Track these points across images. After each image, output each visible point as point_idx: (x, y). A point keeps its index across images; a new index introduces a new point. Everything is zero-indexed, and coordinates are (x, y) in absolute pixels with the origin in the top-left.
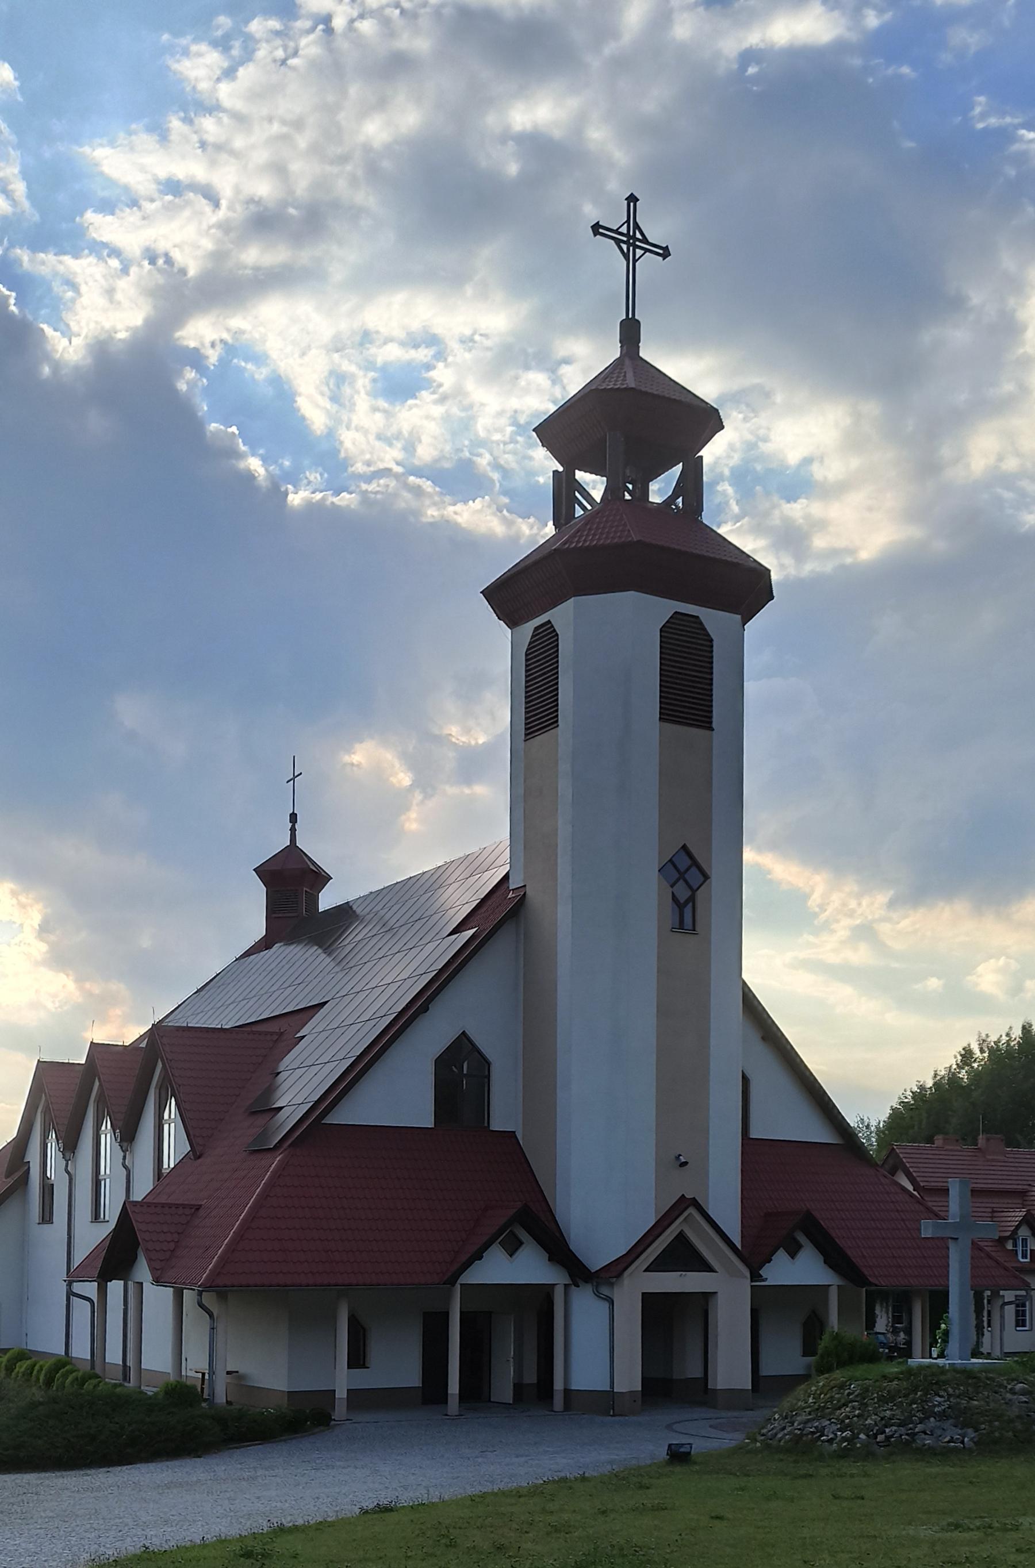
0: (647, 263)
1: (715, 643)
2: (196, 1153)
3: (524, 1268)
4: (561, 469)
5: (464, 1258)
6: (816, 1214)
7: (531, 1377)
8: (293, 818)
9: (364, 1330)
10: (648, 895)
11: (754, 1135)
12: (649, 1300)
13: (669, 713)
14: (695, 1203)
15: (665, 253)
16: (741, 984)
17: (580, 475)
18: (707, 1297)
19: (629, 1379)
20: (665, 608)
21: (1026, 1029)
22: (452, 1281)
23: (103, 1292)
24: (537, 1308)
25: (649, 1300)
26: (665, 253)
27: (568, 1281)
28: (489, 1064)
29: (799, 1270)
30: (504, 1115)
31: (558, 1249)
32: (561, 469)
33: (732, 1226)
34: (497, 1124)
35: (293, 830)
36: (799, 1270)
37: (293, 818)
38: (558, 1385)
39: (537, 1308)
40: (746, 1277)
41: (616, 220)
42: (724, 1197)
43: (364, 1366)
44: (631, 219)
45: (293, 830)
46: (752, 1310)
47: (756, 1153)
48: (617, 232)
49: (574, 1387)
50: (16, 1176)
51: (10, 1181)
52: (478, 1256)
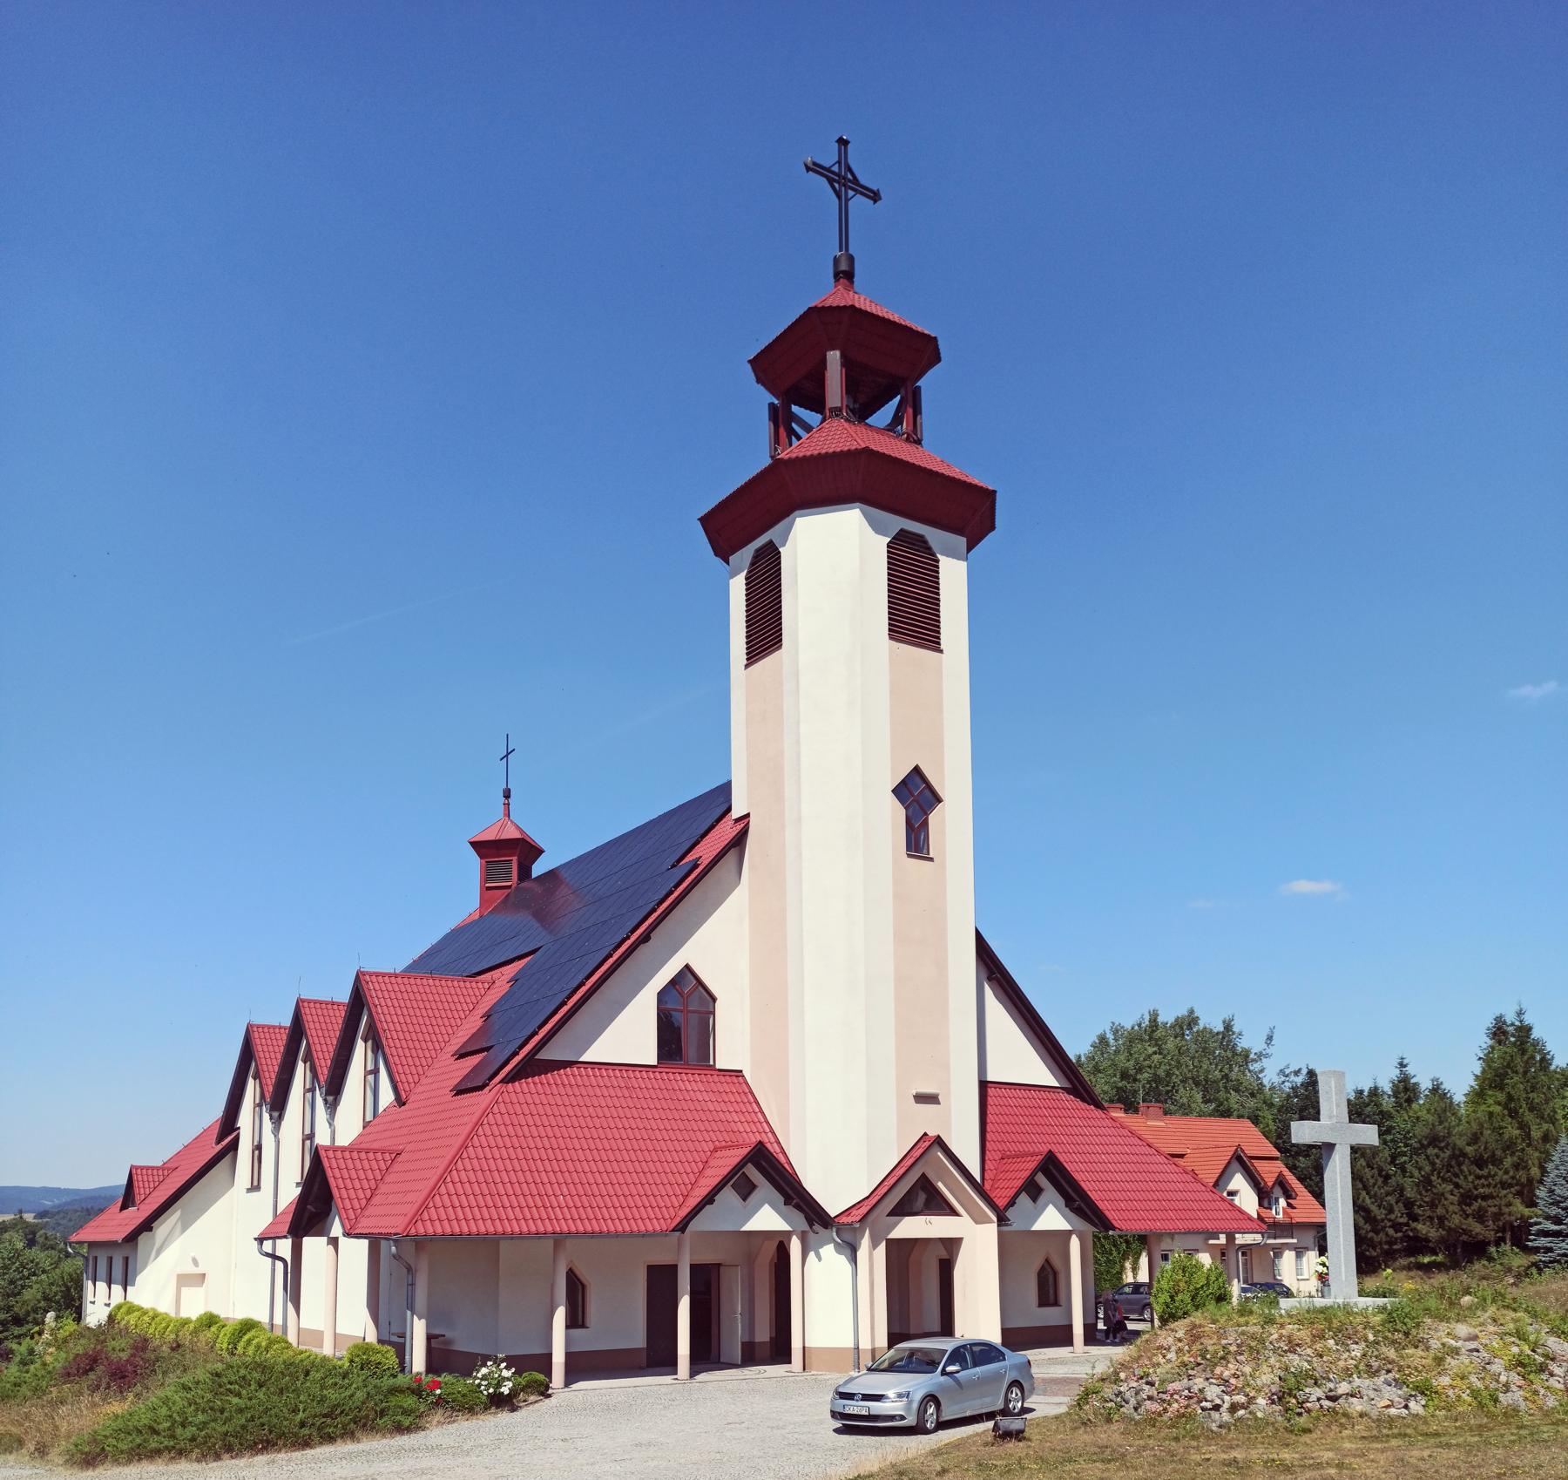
0: (858, 203)
2: (400, 1101)
3: (767, 1218)
5: (693, 1202)
6: (1061, 1157)
7: (763, 1334)
9: (583, 1286)
10: (893, 815)
14: (939, 1142)
15: (875, 196)
16: (724, 808)
18: (951, 1245)
21: (1513, 1051)
22: (682, 1227)
23: (297, 1251)
26: (875, 196)
27: (805, 1227)
30: (732, 1046)
38: (796, 1344)
40: (991, 1221)
41: (829, 158)
43: (583, 1326)
44: (843, 159)
48: (828, 170)
51: (220, 1147)
52: (709, 1199)
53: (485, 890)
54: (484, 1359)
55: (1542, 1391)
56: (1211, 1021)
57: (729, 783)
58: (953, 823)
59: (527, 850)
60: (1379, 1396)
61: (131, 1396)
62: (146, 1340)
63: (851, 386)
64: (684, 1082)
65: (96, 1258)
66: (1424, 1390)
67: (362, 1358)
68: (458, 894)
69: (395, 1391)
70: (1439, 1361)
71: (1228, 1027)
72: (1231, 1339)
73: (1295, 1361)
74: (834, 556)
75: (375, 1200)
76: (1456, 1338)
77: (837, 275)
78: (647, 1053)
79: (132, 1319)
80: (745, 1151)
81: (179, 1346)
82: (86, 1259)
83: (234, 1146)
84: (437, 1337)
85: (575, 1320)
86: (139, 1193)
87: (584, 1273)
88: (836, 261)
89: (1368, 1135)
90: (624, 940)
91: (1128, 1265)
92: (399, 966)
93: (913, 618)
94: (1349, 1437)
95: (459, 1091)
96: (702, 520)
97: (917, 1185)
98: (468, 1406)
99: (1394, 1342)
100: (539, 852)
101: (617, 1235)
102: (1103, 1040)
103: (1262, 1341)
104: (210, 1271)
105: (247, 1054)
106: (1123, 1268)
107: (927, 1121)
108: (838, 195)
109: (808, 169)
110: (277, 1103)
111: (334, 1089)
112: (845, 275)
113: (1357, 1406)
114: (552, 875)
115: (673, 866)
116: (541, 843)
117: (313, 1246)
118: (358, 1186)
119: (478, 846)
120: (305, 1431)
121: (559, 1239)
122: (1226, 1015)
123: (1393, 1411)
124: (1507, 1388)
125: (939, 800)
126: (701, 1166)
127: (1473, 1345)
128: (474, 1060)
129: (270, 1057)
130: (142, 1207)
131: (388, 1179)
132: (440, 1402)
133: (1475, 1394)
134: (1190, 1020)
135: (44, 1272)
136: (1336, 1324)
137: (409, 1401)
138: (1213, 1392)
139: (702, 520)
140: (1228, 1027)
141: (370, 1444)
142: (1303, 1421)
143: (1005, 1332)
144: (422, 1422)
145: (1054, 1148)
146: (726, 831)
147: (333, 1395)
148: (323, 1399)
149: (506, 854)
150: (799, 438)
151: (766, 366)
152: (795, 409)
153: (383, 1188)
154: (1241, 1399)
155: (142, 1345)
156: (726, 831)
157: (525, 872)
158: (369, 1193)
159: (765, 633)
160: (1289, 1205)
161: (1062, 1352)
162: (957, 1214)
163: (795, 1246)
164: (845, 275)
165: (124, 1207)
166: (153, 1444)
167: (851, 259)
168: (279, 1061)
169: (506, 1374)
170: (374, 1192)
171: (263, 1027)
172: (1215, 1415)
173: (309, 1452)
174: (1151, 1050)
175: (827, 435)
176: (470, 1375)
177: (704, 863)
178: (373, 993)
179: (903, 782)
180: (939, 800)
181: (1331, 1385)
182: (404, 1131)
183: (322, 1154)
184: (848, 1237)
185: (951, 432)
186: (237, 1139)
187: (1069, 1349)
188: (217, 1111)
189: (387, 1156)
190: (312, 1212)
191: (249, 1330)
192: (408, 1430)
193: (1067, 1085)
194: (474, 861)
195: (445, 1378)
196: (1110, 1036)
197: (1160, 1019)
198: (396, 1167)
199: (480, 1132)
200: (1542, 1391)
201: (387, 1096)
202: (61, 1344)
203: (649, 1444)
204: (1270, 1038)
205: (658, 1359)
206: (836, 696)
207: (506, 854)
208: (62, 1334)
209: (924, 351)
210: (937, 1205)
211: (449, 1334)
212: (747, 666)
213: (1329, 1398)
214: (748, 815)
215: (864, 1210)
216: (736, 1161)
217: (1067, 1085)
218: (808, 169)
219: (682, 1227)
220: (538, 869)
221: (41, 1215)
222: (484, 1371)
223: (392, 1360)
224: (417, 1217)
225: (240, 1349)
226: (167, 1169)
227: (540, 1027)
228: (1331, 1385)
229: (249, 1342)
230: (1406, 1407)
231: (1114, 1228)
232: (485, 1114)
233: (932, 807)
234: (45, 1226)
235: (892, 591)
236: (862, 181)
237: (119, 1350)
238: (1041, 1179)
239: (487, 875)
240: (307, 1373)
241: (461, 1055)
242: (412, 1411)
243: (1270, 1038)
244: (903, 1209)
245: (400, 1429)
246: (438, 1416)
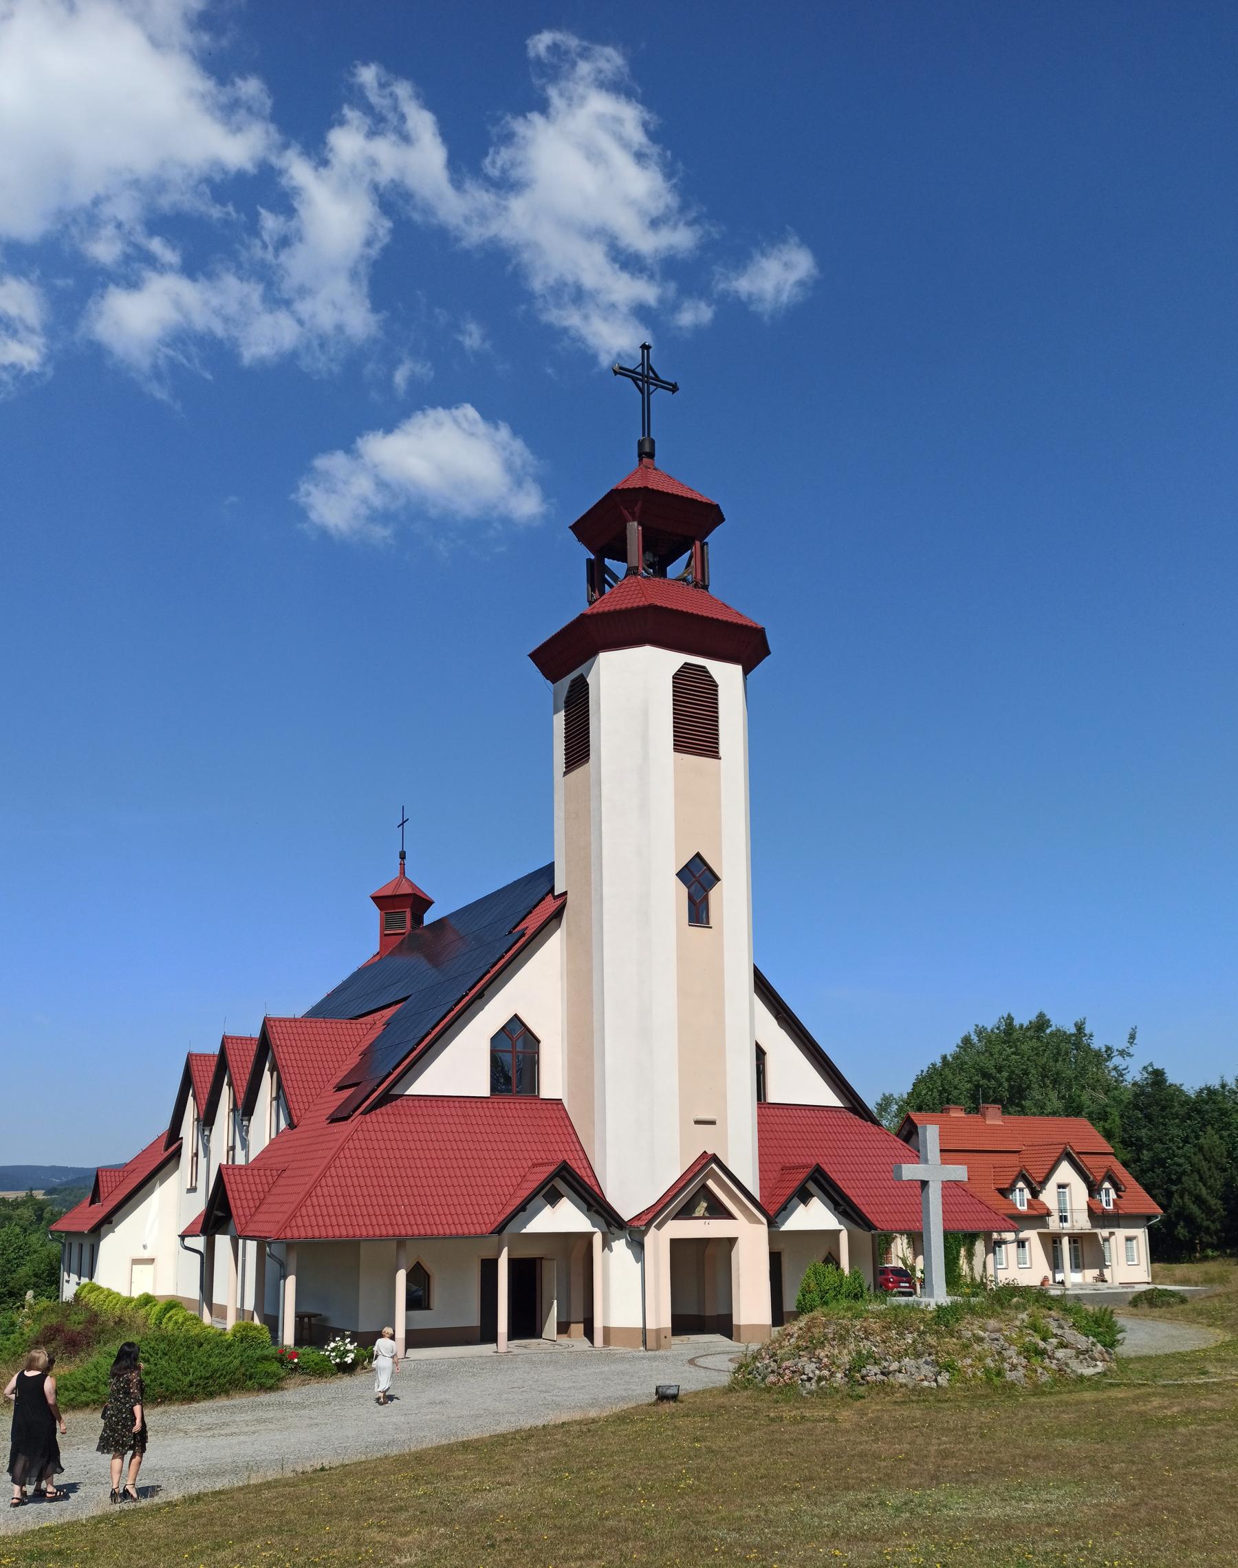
1: (720, 689)
3: (564, 1217)
4: (593, 557)
5: (509, 1210)
6: (824, 1167)
8: (403, 856)
10: (675, 895)
11: (773, 1097)
12: (677, 1245)
13: (681, 745)
14: (715, 1159)
15: (674, 388)
17: (608, 562)
18: (732, 1242)
19: (662, 1318)
20: (675, 660)
22: (500, 1230)
23: (210, 1246)
24: (576, 1251)
25: (677, 1245)
26: (674, 388)
28: (539, 1042)
29: (813, 1216)
30: (552, 1083)
31: (594, 1202)
32: (593, 557)
33: (751, 1181)
34: (545, 1094)
35: (402, 865)
36: (813, 1216)
37: (403, 856)
39: (576, 1251)
42: (744, 1161)
45: (402, 865)
46: (771, 1254)
47: (773, 1118)
49: (612, 1324)
50: (171, 1150)
51: (167, 1154)
53: (384, 936)
54: (340, 1333)
55: (1040, 1370)
56: (1063, 1021)
57: (553, 864)
58: (732, 898)
59: (421, 903)
60: (915, 1372)
61: (78, 1360)
62: (96, 1315)
63: (647, 546)
64: (513, 1108)
65: (70, 1244)
66: (949, 1367)
67: (244, 1335)
68: (359, 940)
69: (266, 1358)
70: (966, 1347)
71: (1080, 1028)
72: (830, 1330)
73: (865, 1346)
74: (633, 684)
75: (262, 1209)
76: (985, 1330)
77: (641, 455)
78: (481, 1086)
79: (92, 1296)
80: (552, 1168)
81: (120, 1320)
82: (64, 1245)
83: (177, 1154)
84: (310, 1316)
85: (416, 1302)
86: (104, 1190)
87: (429, 1266)
88: (640, 444)
89: (959, 1172)
90: (464, 997)
91: (963, 1252)
92: (299, 1011)
93: (695, 729)
94: (889, 1402)
95: (334, 1120)
96: (534, 656)
97: (697, 1190)
98: (321, 1371)
99: (937, 1332)
100: (428, 903)
101: (445, 1237)
102: (967, 1040)
103: (848, 1331)
104: (147, 1257)
105: (187, 1081)
106: (958, 1252)
107: (706, 1141)
108: (641, 391)
109: (616, 373)
110: (207, 1120)
111: (245, 1109)
112: (646, 452)
113: (902, 1378)
114: (440, 924)
115: (510, 932)
116: (706, 492)
117: (223, 1242)
118: (249, 1196)
119: (376, 899)
120: (193, 1389)
121: (401, 1242)
122: (1078, 1019)
123: (926, 1383)
124: (1014, 1367)
125: (718, 879)
126: (519, 1179)
127: (997, 1335)
128: (347, 1093)
129: (204, 1081)
130: (106, 1203)
131: (274, 1191)
132: (296, 1369)
133: (987, 1371)
134: (1041, 1024)
135: (35, 1252)
136: (900, 1319)
137: (274, 1367)
138: (810, 1368)
139: (534, 656)
140: (1080, 1028)
141: (241, 1400)
142: (861, 1390)
143: (675, 1318)
144: (283, 1384)
145: (820, 1160)
146: (550, 905)
147: (214, 1361)
148: (209, 1364)
149: (401, 905)
150: (611, 586)
151: (582, 529)
152: (608, 562)
153: (270, 1199)
154: (826, 1373)
155: (94, 1318)
156: (550, 905)
157: (418, 919)
158: (257, 1203)
159: (579, 749)
160: (1119, 1196)
161: (486, 1349)
162: (734, 1218)
163: (598, 1240)
164: (646, 452)
165: (92, 1202)
166: (84, 1397)
167: (652, 442)
168: (214, 1080)
169: (349, 1347)
170: (262, 1202)
171: (200, 1055)
172: (807, 1384)
173: (195, 1405)
174: (1009, 1051)
175: (630, 587)
176: (322, 1348)
177: (529, 933)
178: (276, 1040)
179: (686, 866)
180: (718, 879)
181: (886, 1364)
182: (292, 1151)
183: (224, 1171)
184: (637, 1237)
185: (731, 577)
186: (180, 1147)
187: (492, 1347)
188: (165, 1125)
189: (275, 1173)
190: (217, 1218)
191: (172, 1308)
192: (271, 1389)
193: (848, 1105)
194: (375, 913)
195: (306, 1349)
196: (975, 1039)
197: (1016, 1023)
198: (281, 1181)
199: (342, 1155)
200: (1040, 1370)
201: (283, 1125)
202: (36, 1317)
203: (441, 1402)
204: (1132, 1037)
205: (487, 1334)
206: (648, 785)
207: (401, 905)
208: (38, 1308)
209: (710, 516)
210: (718, 1211)
211: (325, 1313)
212: (565, 773)
213: (882, 1373)
214: (566, 893)
215: (650, 1216)
216: (543, 1177)
217: (848, 1105)
218: (616, 373)
219: (500, 1230)
220: (429, 917)
221: (49, 1192)
222: (332, 1345)
223: (267, 1336)
224: (286, 1225)
225: (163, 1326)
226: (123, 1170)
227: (394, 1069)
228: (886, 1364)
229: (171, 1317)
230: (936, 1381)
231: (876, 1229)
232: (347, 1140)
233: (712, 885)
234: (52, 1202)
235: (676, 713)
236: (662, 377)
237: (76, 1323)
238: (812, 1187)
239: (386, 924)
240: (201, 1345)
241: (340, 1088)
242: (275, 1375)
243: (1132, 1037)
244: (685, 1213)
245: (264, 1388)
246: (297, 1379)
